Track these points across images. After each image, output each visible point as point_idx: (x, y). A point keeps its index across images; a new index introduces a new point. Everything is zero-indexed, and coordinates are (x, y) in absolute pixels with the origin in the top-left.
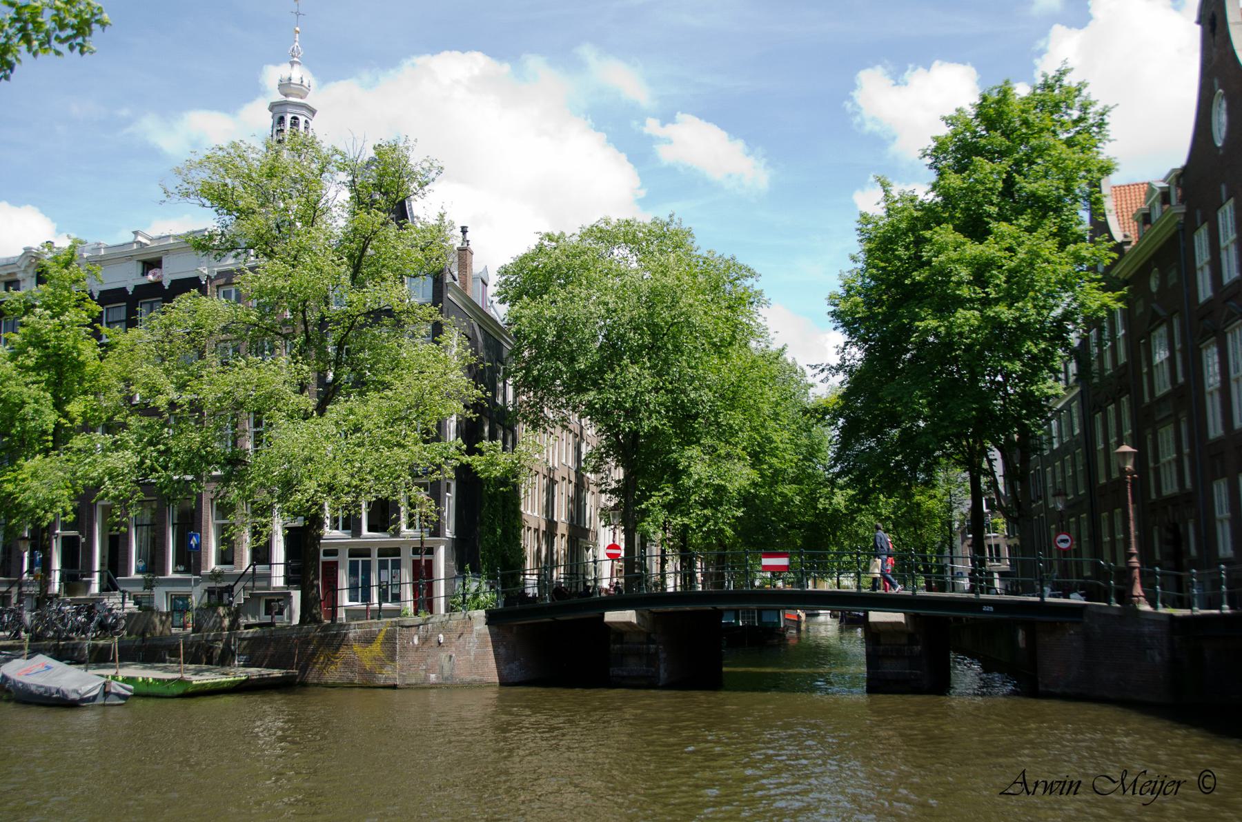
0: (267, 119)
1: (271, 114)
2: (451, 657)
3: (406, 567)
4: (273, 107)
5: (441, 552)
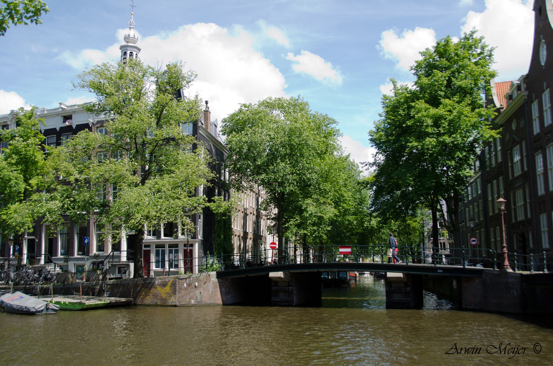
0: (119, 53)
1: (121, 51)
2: (201, 292)
3: (181, 253)
4: (121, 48)
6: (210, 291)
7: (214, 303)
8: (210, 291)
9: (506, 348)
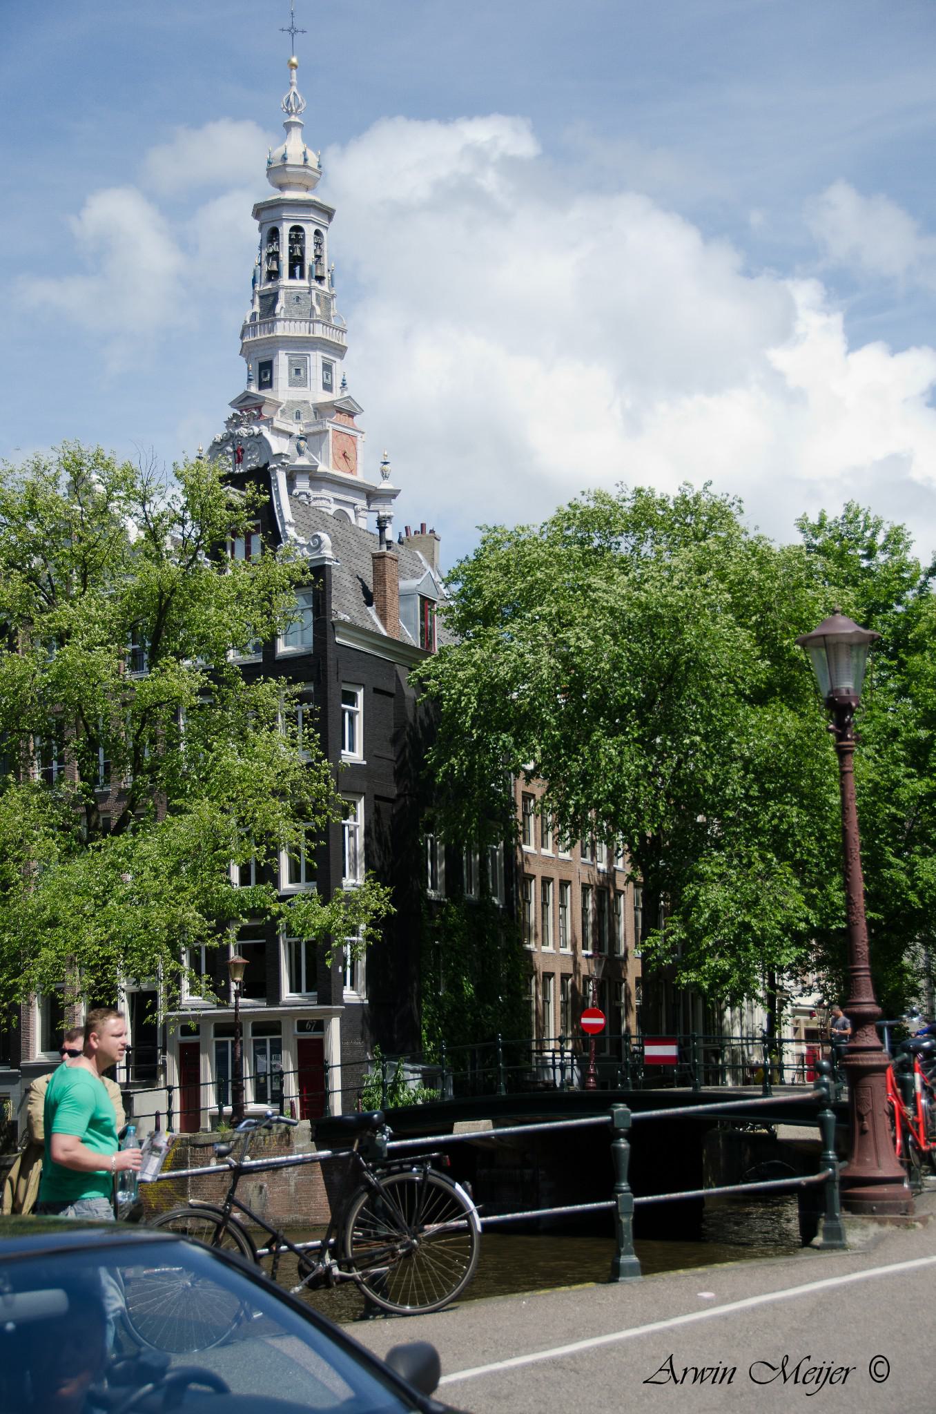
0: (252, 231)
1: (257, 223)
2: (261, 1188)
3: (288, 1049)
5: (335, 1025)
6: (293, 1184)
7: (305, 1222)
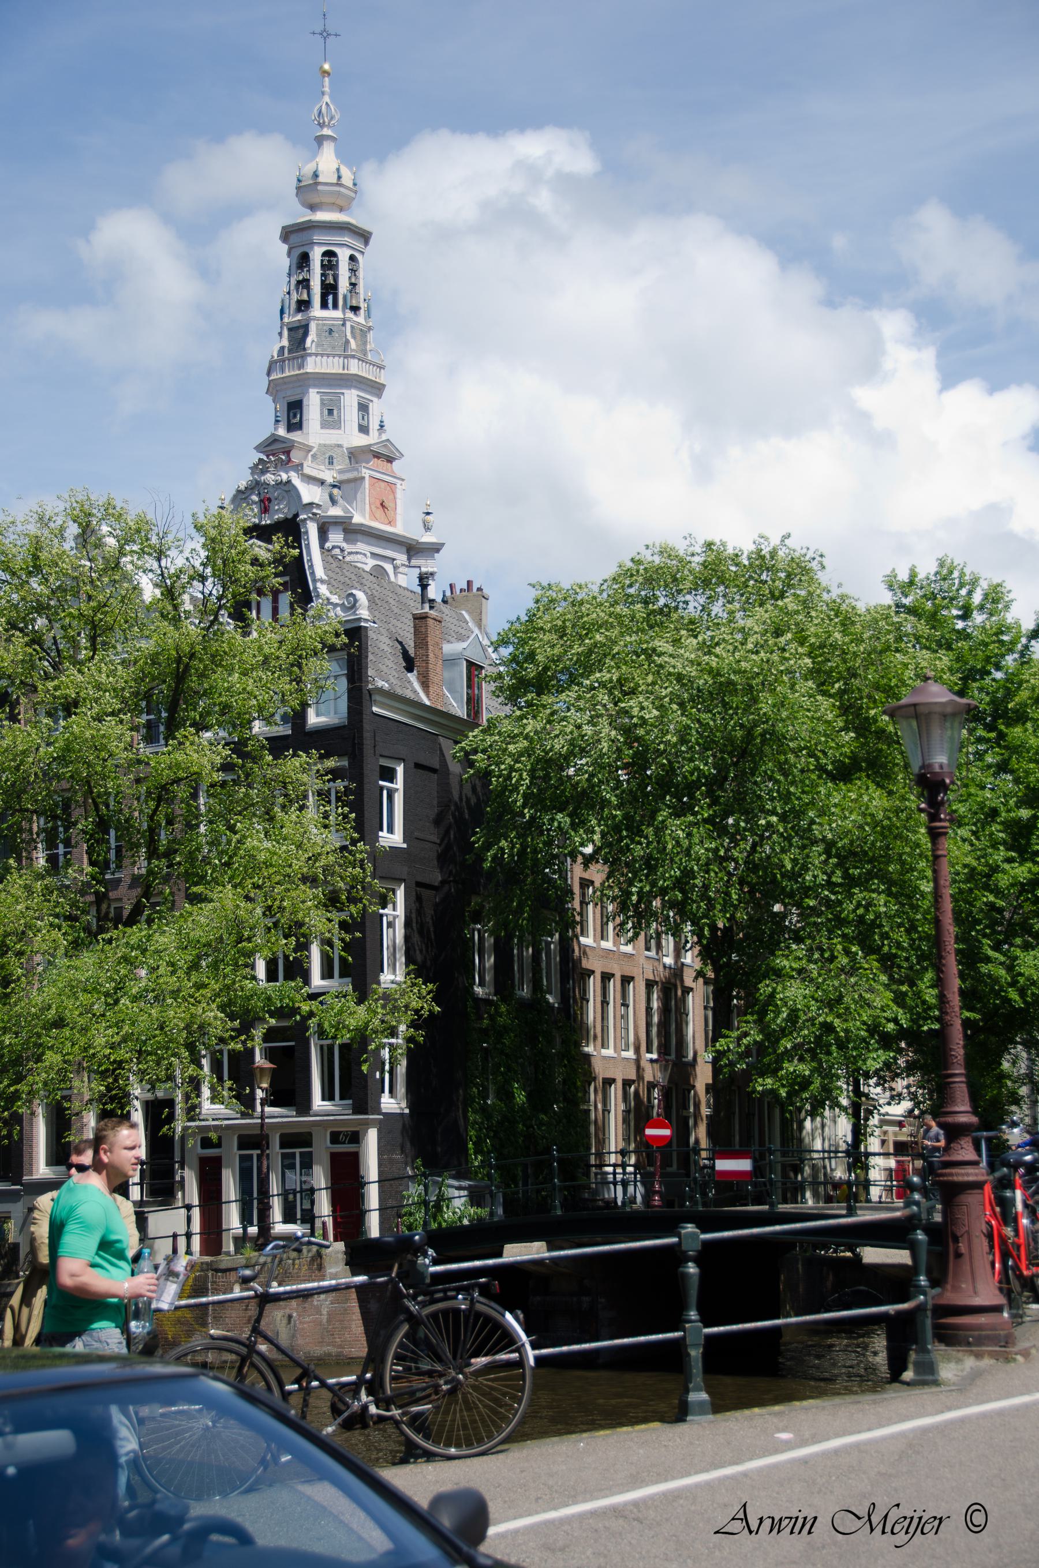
0: (280, 256)
2: (290, 1317)
3: (319, 1163)
4: (288, 234)
6: (325, 1312)
7: (338, 1355)
8: (325, 1312)
9: (886, 1517)
